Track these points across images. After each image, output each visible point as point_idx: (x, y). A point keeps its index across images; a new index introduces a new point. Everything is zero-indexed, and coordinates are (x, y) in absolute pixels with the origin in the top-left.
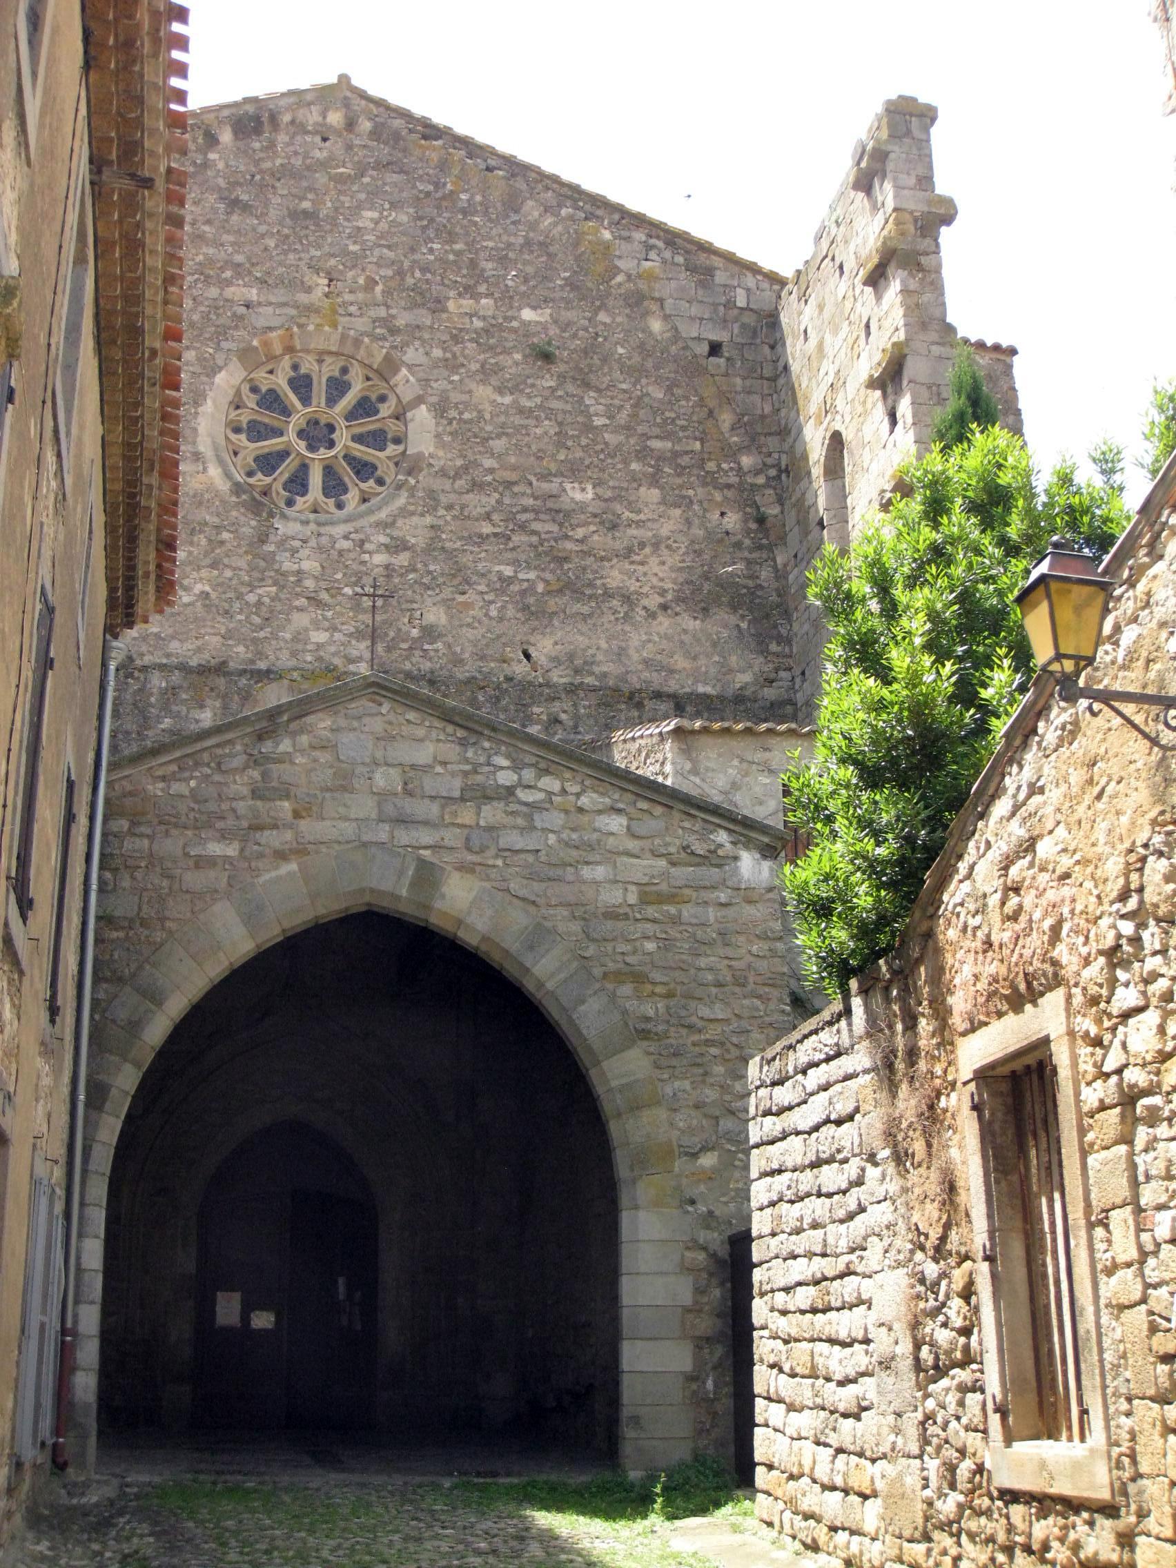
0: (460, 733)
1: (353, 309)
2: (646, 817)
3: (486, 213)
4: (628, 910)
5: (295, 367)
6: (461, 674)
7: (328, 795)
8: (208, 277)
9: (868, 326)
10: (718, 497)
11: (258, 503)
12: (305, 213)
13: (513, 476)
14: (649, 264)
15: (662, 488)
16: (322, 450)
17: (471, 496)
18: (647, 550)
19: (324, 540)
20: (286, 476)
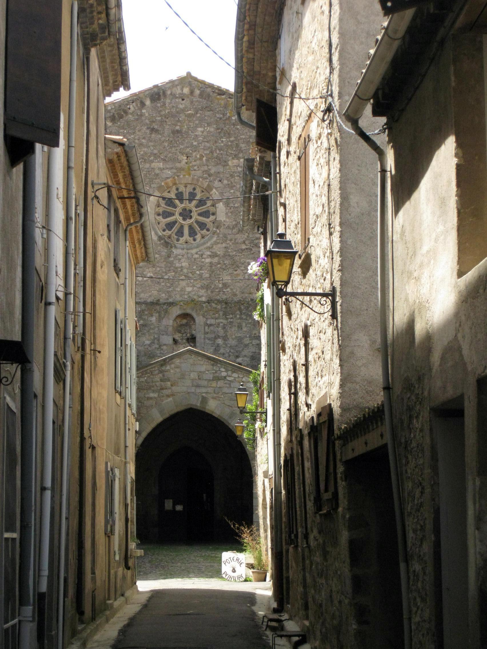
0: (212, 363)
1: (196, 168)
5: (177, 189)
6: (236, 299)
7: (179, 380)
8: (145, 160)
11: (167, 243)
12: (178, 131)
16: (188, 220)
17: (238, 235)
19: (189, 255)
20: (176, 230)
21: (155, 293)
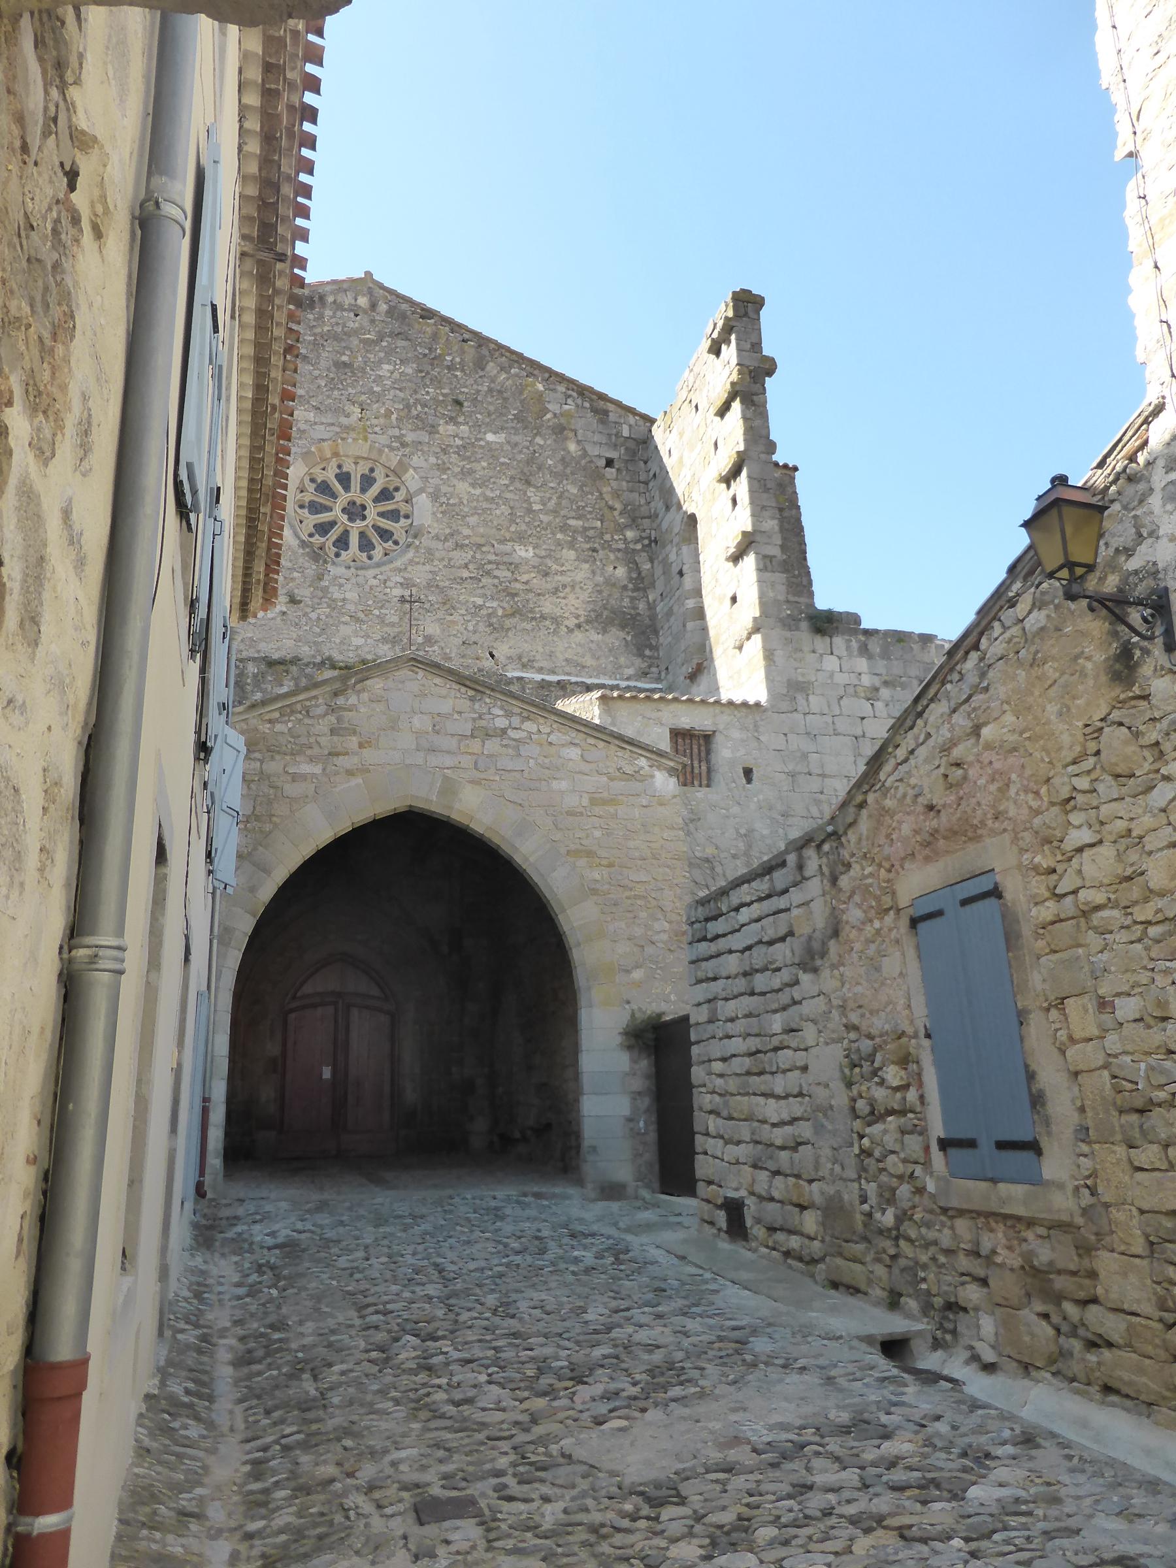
0: (471, 693)
1: (377, 429)
2: (593, 748)
3: (463, 370)
4: (582, 810)
5: (340, 467)
7: (382, 733)
9: (716, 444)
10: (612, 556)
11: (317, 555)
12: (344, 363)
13: (482, 541)
14: (567, 407)
15: (576, 550)
18: (568, 590)
19: (361, 580)
20: (334, 538)
21: (290, 643)
